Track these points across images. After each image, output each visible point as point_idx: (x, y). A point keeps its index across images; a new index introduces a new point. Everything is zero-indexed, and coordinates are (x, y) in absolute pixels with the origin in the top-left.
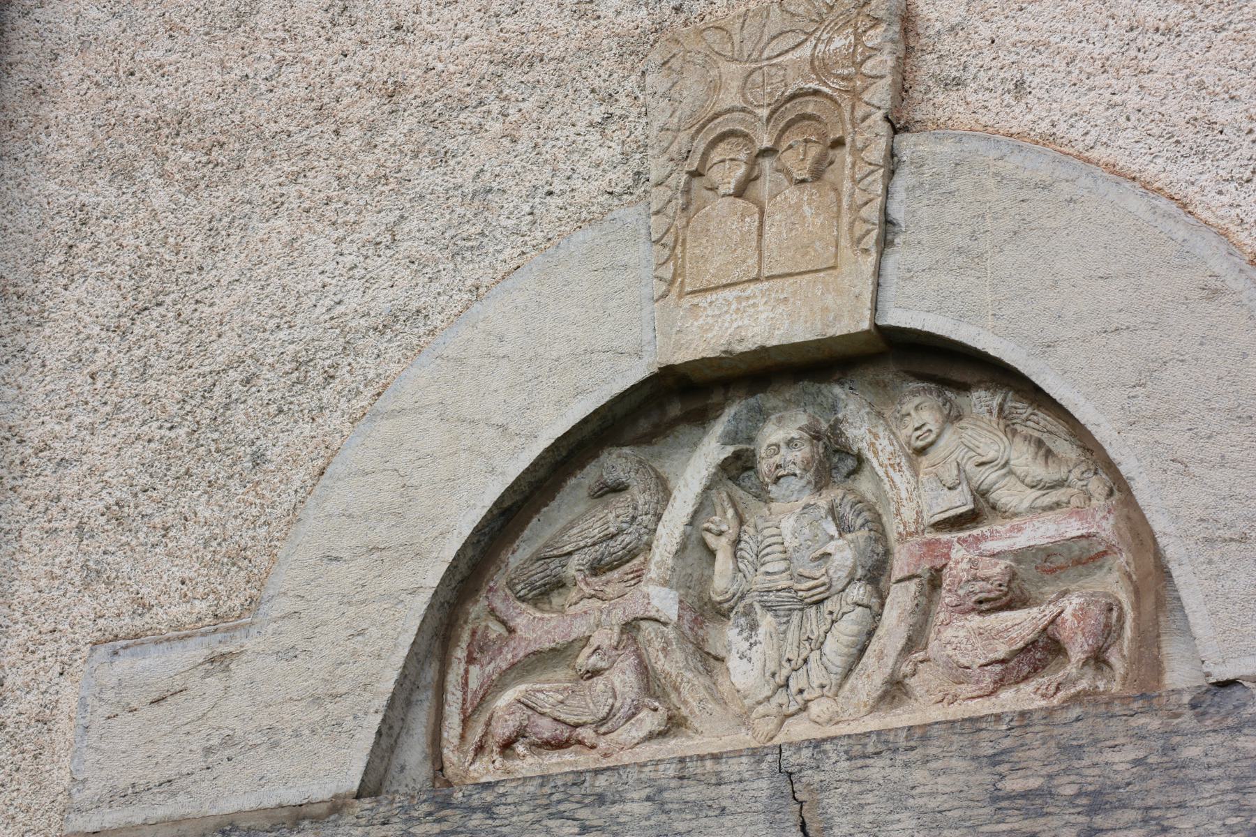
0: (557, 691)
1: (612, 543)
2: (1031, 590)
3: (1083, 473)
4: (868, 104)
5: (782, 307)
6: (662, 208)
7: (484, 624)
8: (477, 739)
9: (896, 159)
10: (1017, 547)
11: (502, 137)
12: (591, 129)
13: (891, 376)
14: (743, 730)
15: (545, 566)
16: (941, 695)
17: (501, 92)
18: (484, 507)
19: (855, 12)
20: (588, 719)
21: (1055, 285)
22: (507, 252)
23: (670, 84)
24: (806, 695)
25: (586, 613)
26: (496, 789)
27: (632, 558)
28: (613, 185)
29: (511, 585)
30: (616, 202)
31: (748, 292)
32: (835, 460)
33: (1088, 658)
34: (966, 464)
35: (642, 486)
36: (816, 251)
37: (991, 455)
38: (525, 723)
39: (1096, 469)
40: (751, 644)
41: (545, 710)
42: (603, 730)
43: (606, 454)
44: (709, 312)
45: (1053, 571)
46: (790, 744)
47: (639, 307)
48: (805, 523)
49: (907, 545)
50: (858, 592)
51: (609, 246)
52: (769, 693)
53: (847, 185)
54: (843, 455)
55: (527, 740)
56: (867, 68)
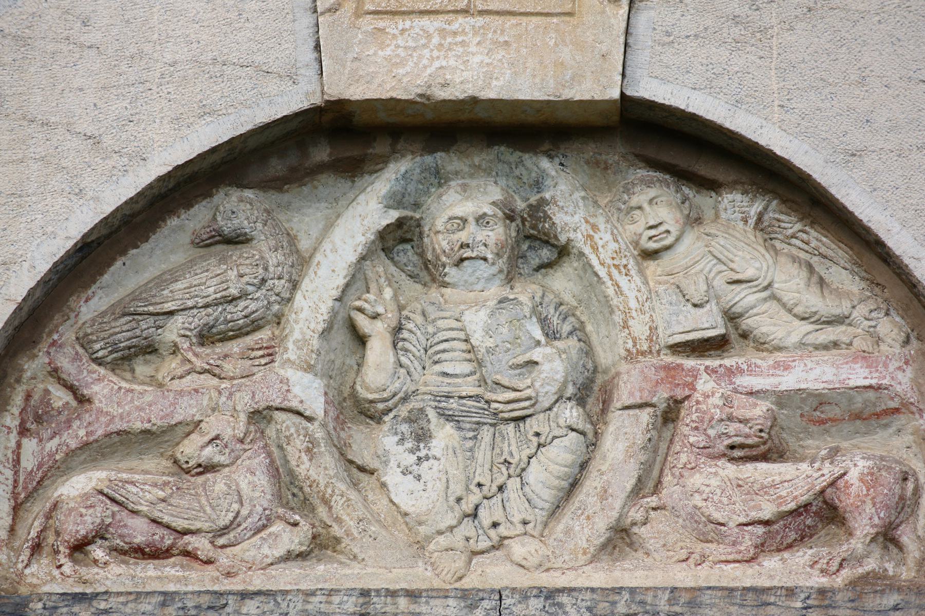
0: (155, 485)
1: (230, 308)
2: (792, 443)
3: (871, 311)
7: (41, 386)
8: (33, 534)
10: (783, 387)
13: (616, 157)
14: (420, 564)
15: (134, 324)
16: (683, 554)
18: (68, 238)
20: (206, 526)
21: (862, 81)
24: (502, 530)
25: (196, 391)
26: (95, 603)
27: (254, 331)
29: (84, 341)
31: (455, 26)
32: (525, 247)
33: (877, 534)
34: (714, 278)
35: (272, 243)
37: (749, 273)
38: (108, 521)
39: (888, 310)
40: (419, 459)
41: (140, 508)
42: (221, 541)
43: (221, 194)
44: (400, 42)
45: (822, 422)
46: (514, 590)
47: (290, 17)
48: (502, 320)
49: (638, 366)
50: (570, 413)
52: (454, 522)
54: (537, 243)
55: (107, 543)
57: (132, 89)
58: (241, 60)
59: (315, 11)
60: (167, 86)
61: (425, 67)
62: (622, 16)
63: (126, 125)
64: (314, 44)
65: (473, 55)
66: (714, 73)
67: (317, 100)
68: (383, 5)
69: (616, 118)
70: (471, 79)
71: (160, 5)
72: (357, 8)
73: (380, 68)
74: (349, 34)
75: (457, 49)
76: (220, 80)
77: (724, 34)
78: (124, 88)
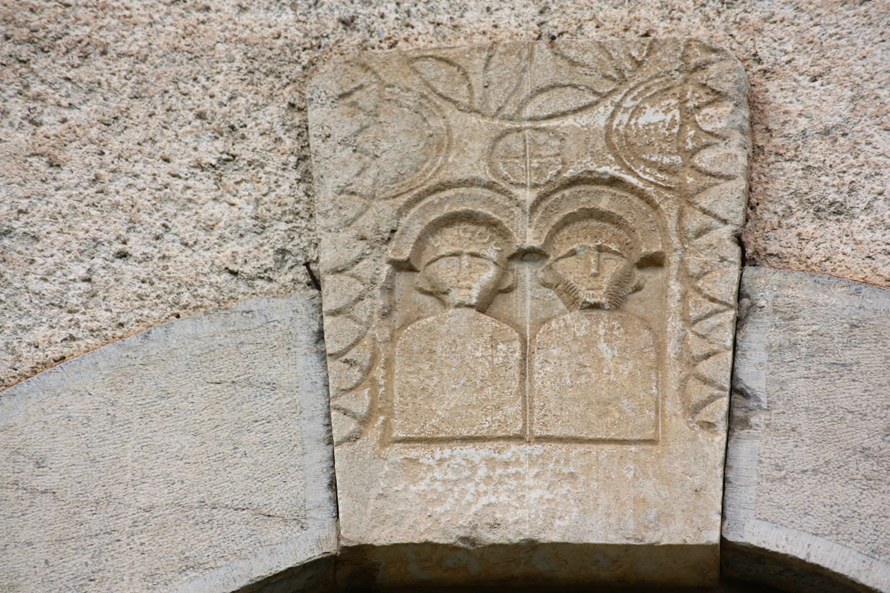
4: (705, 212)
5: (566, 487)
6: (346, 306)
9: (746, 302)
11: (33, 155)
12: (198, 171)
17: (27, 87)
19: (680, 77)
22: (40, 334)
23: (356, 127)
28: (240, 261)
30: (243, 288)
31: (507, 455)
36: (621, 412)
44: (437, 474)
47: (299, 449)
51: (243, 349)
53: (674, 325)
56: (705, 159)
57: (95, 540)
58: (236, 502)
59: (330, 442)
60: (140, 536)
61: (469, 504)
62: (719, 443)
63: (86, 585)
64: (328, 481)
65: (530, 489)
66: (840, 516)
67: (332, 548)
68: (416, 431)
69: (714, 574)
70: (527, 519)
71: (135, 439)
72: (382, 435)
73: (411, 506)
74: (373, 466)
75: (510, 482)
76: (208, 526)
77: (851, 470)
78: (85, 540)
